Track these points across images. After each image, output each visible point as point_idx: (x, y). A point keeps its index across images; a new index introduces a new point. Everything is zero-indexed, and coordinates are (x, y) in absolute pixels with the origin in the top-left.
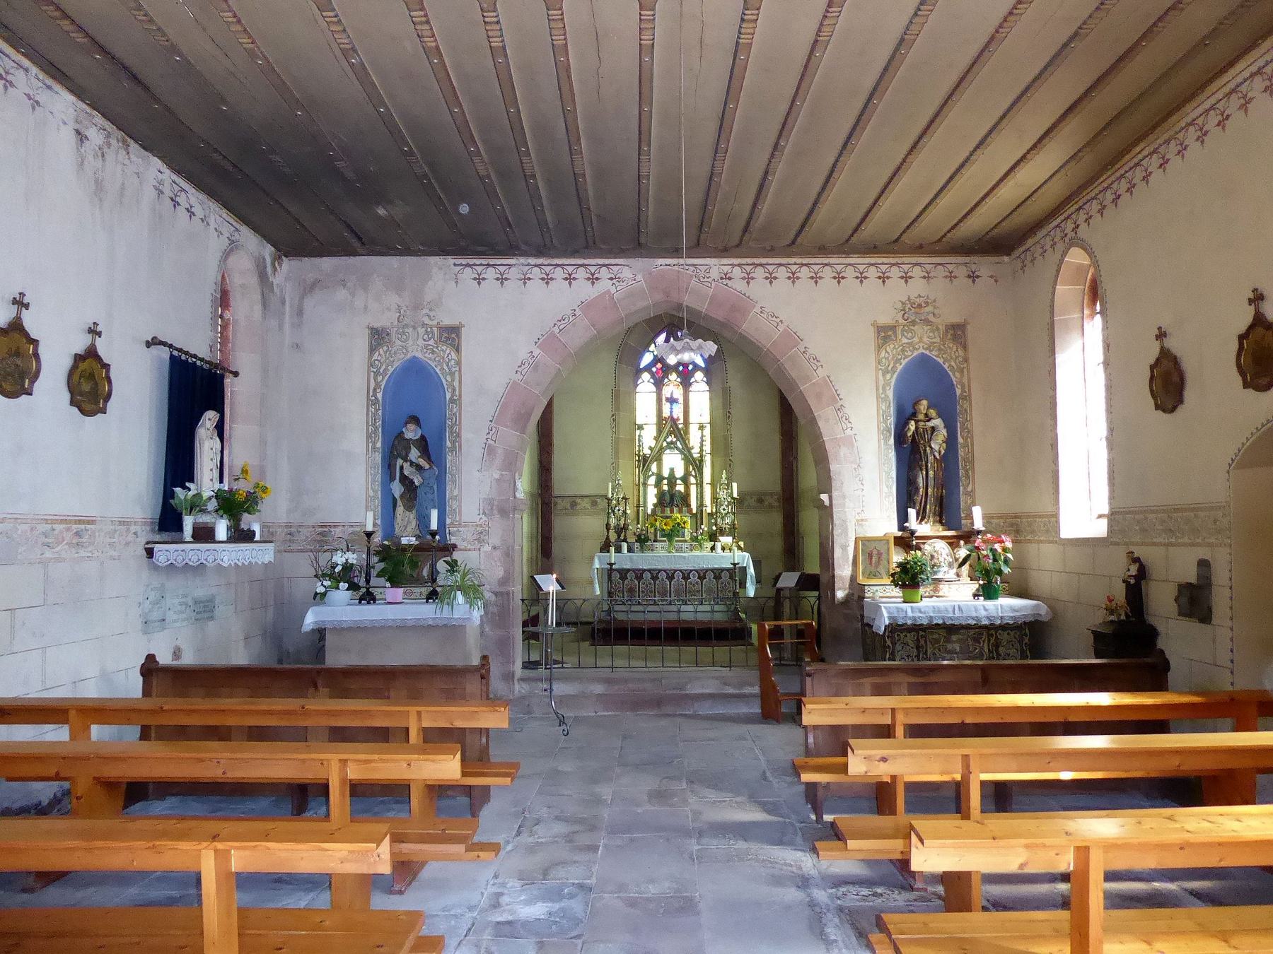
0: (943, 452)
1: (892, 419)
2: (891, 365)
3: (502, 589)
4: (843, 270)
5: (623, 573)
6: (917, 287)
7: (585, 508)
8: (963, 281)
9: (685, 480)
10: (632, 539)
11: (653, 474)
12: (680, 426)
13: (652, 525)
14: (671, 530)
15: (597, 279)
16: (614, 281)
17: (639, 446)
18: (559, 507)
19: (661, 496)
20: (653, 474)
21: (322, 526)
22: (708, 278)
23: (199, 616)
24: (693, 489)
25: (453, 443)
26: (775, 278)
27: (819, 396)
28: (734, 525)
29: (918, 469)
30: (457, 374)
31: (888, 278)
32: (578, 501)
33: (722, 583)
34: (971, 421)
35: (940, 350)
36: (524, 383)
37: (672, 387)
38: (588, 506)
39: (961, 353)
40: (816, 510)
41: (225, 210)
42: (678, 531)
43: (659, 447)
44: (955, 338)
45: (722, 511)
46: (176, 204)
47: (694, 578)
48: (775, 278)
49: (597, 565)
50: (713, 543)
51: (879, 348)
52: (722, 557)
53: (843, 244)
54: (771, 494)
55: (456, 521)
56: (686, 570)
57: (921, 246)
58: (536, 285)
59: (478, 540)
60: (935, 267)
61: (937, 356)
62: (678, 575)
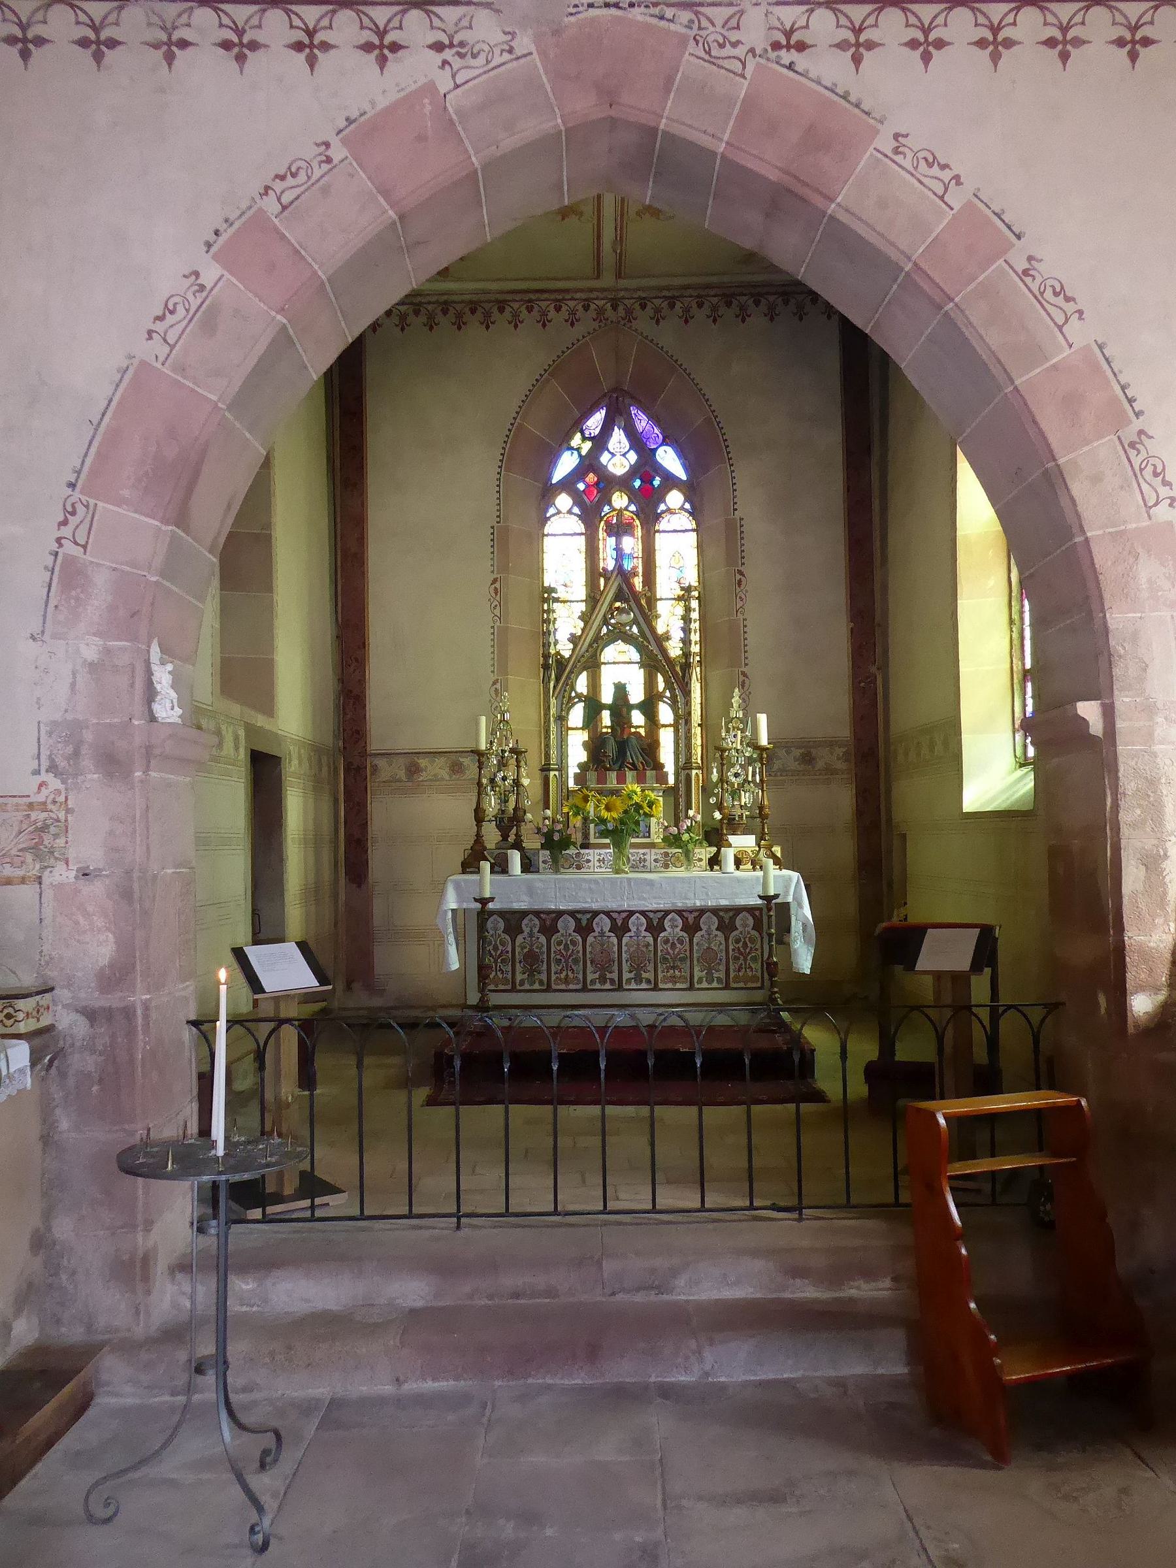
3: (112, 1000)
4: (1147, 18)
5: (513, 920)
7: (436, 778)
9: (649, 707)
10: (532, 842)
13: (578, 810)
14: (622, 822)
15: (395, 47)
16: (448, 54)
19: (595, 747)
20: (579, 696)
22: (735, 45)
26: (940, 44)
27: (1071, 403)
28: (761, 808)
32: (423, 762)
33: (738, 941)
36: (174, 370)
38: (444, 773)
42: (637, 823)
45: (733, 779)
47: (673, 929)
48: (940, 44)
49: (451, 902)
50: (714, 849)
52: (739, 880)
54: (831, 744)
56: (655, 912)
59: (36, 850)
62: (637, 924)
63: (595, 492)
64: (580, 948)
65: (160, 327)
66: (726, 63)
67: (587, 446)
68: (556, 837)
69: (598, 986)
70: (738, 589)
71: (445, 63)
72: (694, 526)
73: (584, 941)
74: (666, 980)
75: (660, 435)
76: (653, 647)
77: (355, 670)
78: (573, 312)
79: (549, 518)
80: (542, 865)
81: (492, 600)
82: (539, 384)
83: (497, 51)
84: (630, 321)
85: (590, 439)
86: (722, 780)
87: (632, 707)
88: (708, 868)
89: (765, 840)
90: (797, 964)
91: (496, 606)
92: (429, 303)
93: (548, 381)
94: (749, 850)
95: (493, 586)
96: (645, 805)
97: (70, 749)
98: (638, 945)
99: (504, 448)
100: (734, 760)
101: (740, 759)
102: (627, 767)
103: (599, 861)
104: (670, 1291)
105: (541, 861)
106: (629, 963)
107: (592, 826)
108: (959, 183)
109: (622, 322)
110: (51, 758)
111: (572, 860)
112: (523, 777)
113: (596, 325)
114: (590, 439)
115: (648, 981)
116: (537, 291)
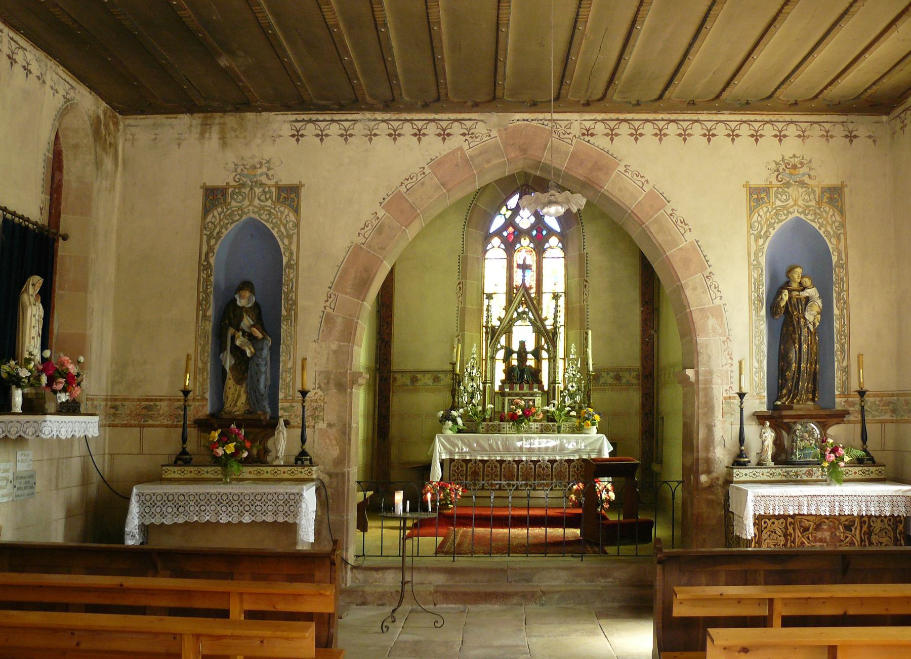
0: (817, 324)
1: (764, 288)
2: (764, 229)
3: (338, 470)
4: (714, 127)
6: (792, 148)
7: (426, 385)
8: (839, 141)
9: (536, 354)
11: (502, 347)
12: (533, 295)
16: (467, 137)
17: (488, 316)
18: (398, 383)
19: (509, 371)
21: (147, 400)
22: (569, 134)
23: (20, 492)
24: (545, 365)
25: (289, 310)
29: (791, 342)
30: (295, 237)
31: (761, 136)
32: (419, 376)
34: (847, 291)
35: (815, 214)
37: (525, 252)
38: (430, 382)
39: (838, 218)
40: (680, 385)
41: (61, 68)
43: (509, 317)
44: (831, 201)
46: (12, 61)
51: (751, 211)
53: (714, 99)
54: (629, 370)
55: (290, 396)
57: (796, 103)
58: (382, 143)
60: (811, 125)
61: (813, 221)
64: (499, 470)
65: (362, 232)
66: (566, 140)
67: (510, 213)
71: (466, 140)
72: (564, 256)
76: (539, 324)
79: (488, 250)
83: (485, 136)
85: (510, 210)
97: (326, 381)
98: (526, 468)
99: (466, 216)
104: (531, 581)
108: (648, 183)
110: (319, 384)
114: (510, 210)
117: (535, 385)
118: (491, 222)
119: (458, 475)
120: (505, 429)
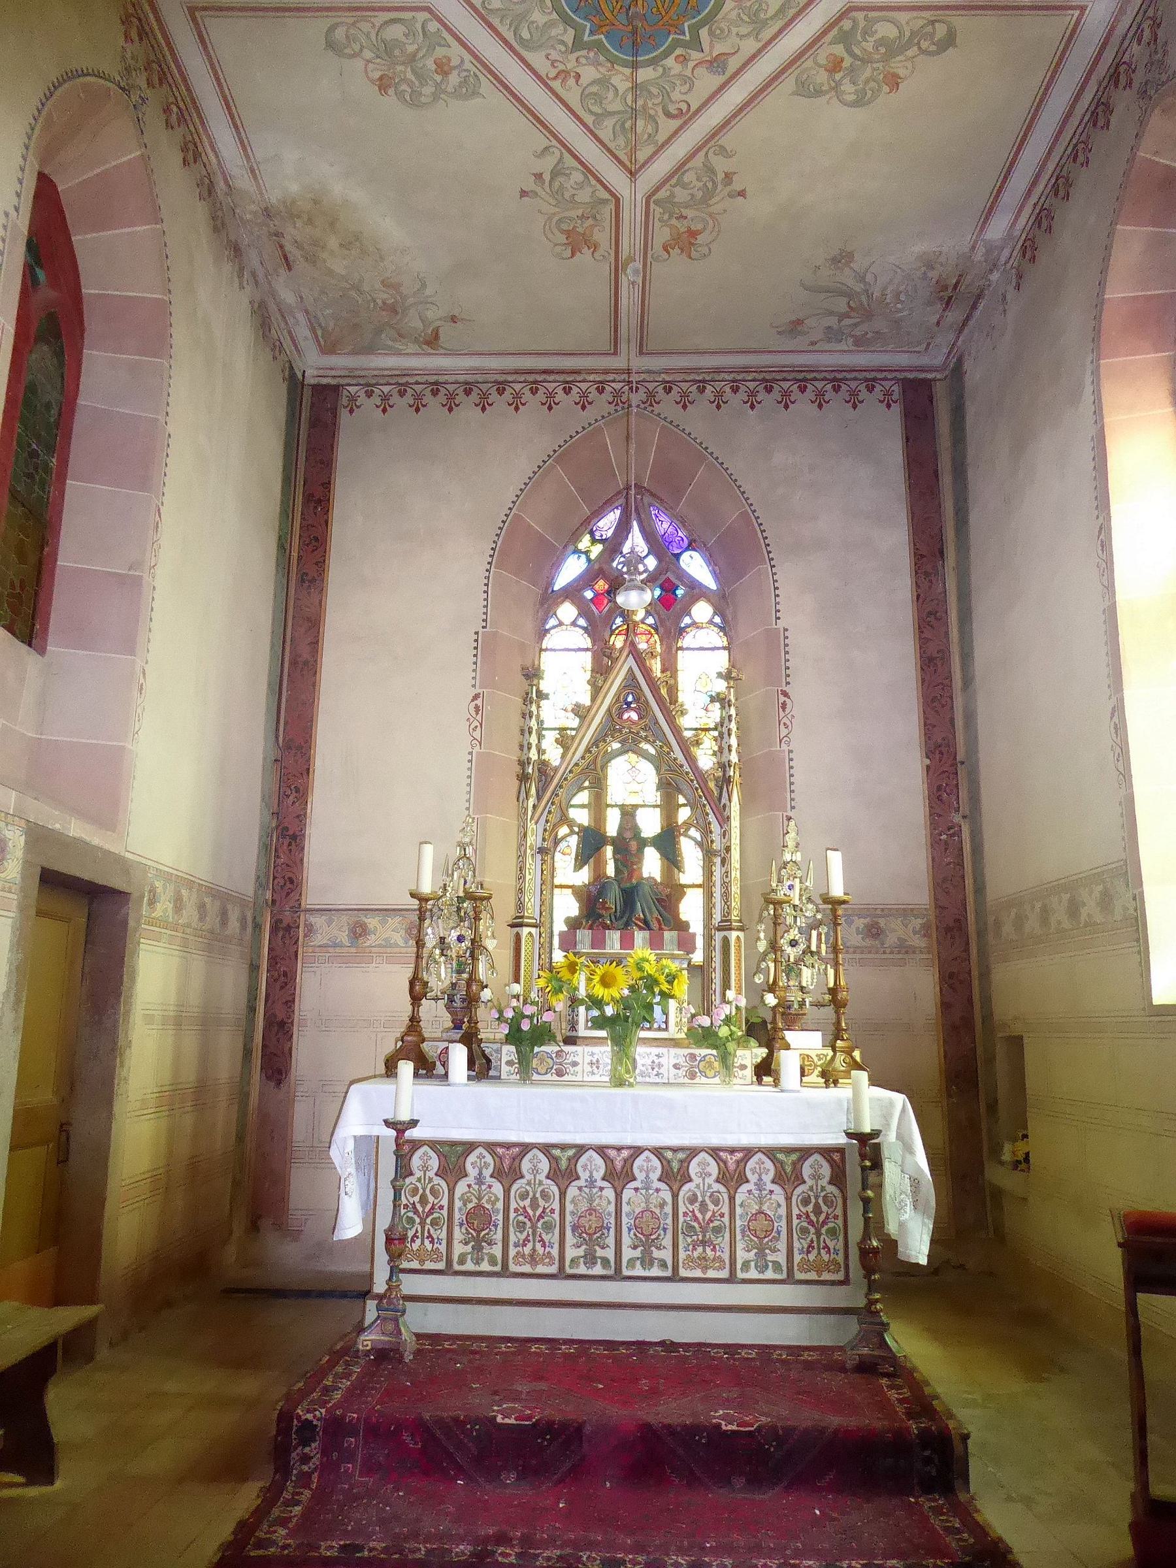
7: (388, 944)
9: (667, 842)
10: (491, 1031)
18: (319, 939)
32: (372, 922)
42: (649, 1007)
54: (906, 912)
56: (675, 1150)
62: (647, 1168)
63: (606, 601)
64: (556, 1206)
67: (597, 550)
68: (525, 1026)
69: (582, 1270)
70: (782, 714)
73: (563, 1195)
74: (691, 1262)
75: (685, 539)
77: (294, 803)
78: (584, 395)
79: (547, 631)
80: (505, 1069)
81: (472, 720)
82: (541, 471)
84: (651, 405)
85: (602, 541)
86: (774, 946)
87: (643, 843)
88: (755, 1079)
89: (843, 1040)
90: (907, 1248)
91: (476, 727)
92: (417, 383)
93: (552, 467)
94: (813, 1054)
95: (474, 703)
96: (662, 979)
100: (789, 920)
101: (798, 919)
102: (636, 924)
103: (592, 1063)
105: (504, 1060)
106: (632, 1233)
107: (582, 1009)
109: (642, 406)
111: (549, 1060)
112: (487, 937)
113: (612, 407)
114: (602, 541)
115: (663, 1265)
116: (545, 372)
117: (667, 935)
118: (557, 565)
119: (423, 1224)
120: (578, 1068)
